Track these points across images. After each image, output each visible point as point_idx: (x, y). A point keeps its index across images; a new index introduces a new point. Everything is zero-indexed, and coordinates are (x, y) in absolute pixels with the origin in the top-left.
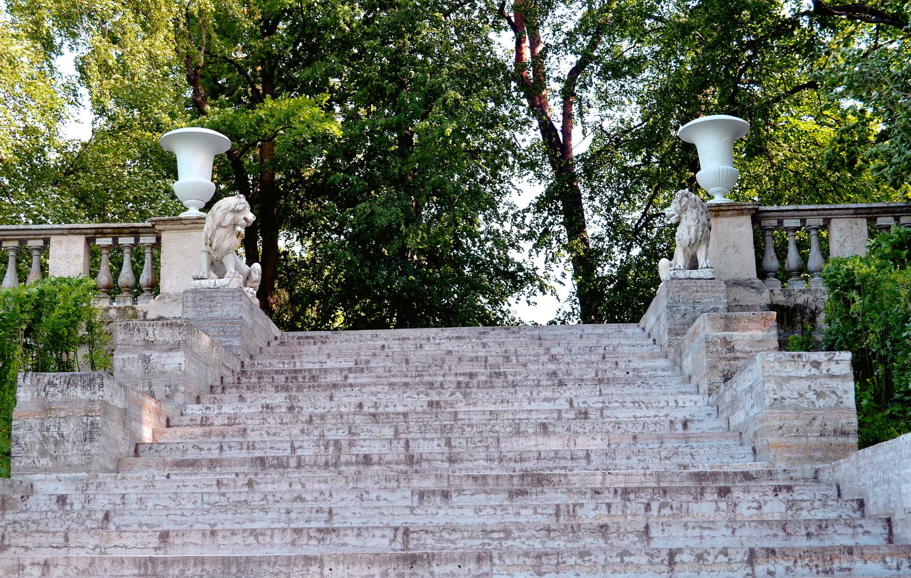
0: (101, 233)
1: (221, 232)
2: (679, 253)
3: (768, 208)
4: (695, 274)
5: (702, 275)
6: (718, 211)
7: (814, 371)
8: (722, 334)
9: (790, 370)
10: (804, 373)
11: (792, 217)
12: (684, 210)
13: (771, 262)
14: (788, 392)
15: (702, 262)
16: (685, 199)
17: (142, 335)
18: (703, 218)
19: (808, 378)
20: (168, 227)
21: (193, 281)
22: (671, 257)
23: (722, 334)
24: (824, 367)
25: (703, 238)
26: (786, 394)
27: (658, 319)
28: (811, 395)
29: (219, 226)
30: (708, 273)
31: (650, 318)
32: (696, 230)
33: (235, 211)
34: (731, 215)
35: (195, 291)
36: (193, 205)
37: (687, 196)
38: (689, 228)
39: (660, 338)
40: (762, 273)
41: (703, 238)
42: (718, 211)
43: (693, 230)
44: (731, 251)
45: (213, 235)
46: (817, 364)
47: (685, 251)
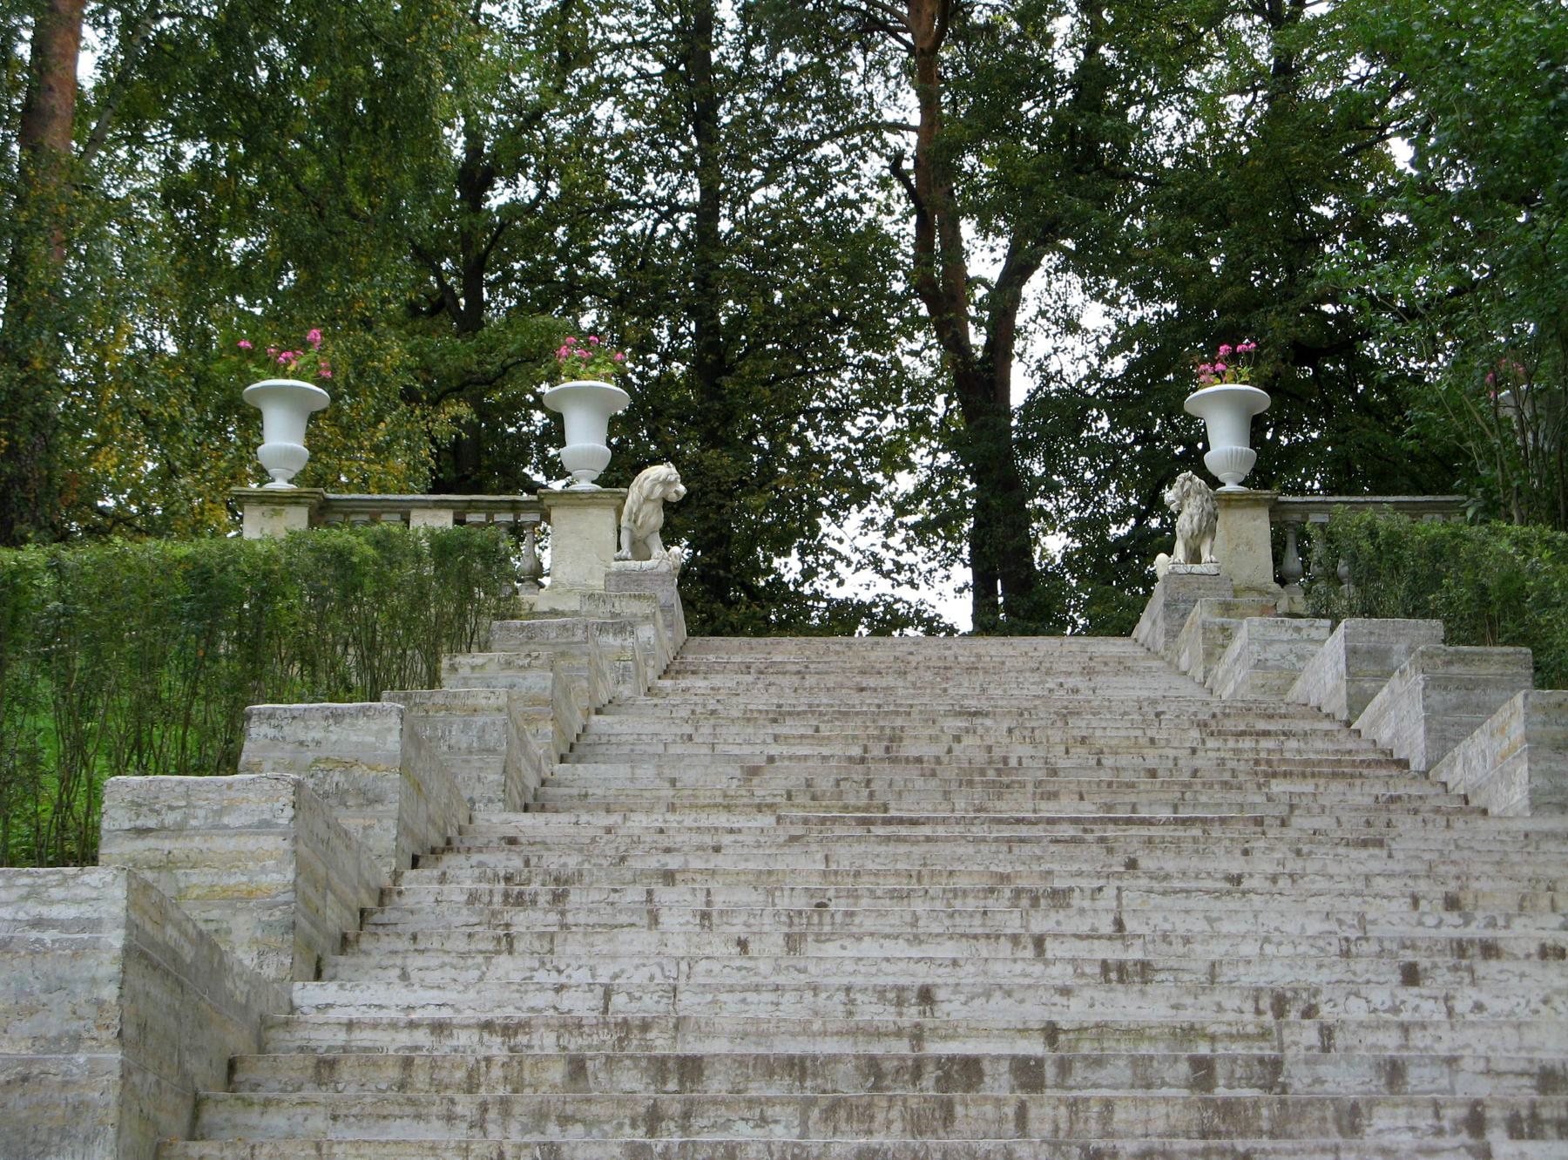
0: (472, 506)
1: (648, 508)
2: (1179, 547)
3: (1290, 498)
4: (1197, 568)
5: (1205, 570)
6: (1229, 501)
7: (1295, 636)
8: (1218, 620)
9: (1273, 633)
10: (1286, 637)
11: (1320, 511)
12: (1187, 495)
13: (1293, 562)
14: (1271, 654)
15: (1206, 556)
16: (1188, 483)
17: (609, 607)
18: (1209, 507)
19: (1289, 641)
20: (561, 501)
21: (614, 564)
22: (1170, 552)
23: (1218, 620)
24: (1304, 633)
25: (1207, 529)
26: (1269, 655)
27: (1154, 623)
28: (1292, 658)
29: (647, 499)
30: (1212, 569)
31: (1144, 627)
32: (1200, 520)
33: (666, 483)
34: (1244, 507)
35: (619, 574)
36: (584, 476)
37: (1190, 479)
38: (1192, 516)
39: (1154, 644)
40: (1282, 580)
41: (1207, 529)
42: (1229, 501)
43: (1196, 519)
44: (1243, 548)
45: (639, 510)
46: (1298, 629)
47: (1186, 545)
